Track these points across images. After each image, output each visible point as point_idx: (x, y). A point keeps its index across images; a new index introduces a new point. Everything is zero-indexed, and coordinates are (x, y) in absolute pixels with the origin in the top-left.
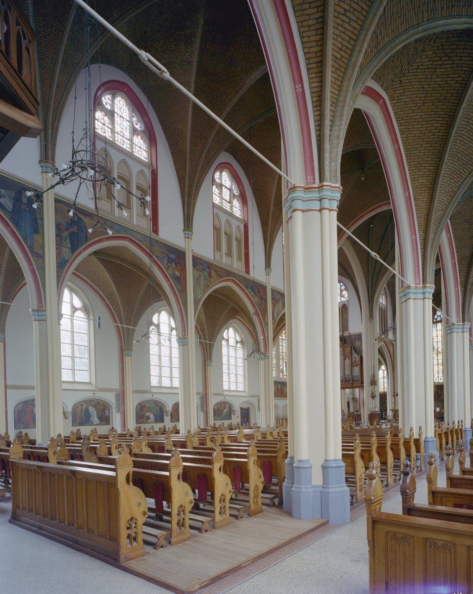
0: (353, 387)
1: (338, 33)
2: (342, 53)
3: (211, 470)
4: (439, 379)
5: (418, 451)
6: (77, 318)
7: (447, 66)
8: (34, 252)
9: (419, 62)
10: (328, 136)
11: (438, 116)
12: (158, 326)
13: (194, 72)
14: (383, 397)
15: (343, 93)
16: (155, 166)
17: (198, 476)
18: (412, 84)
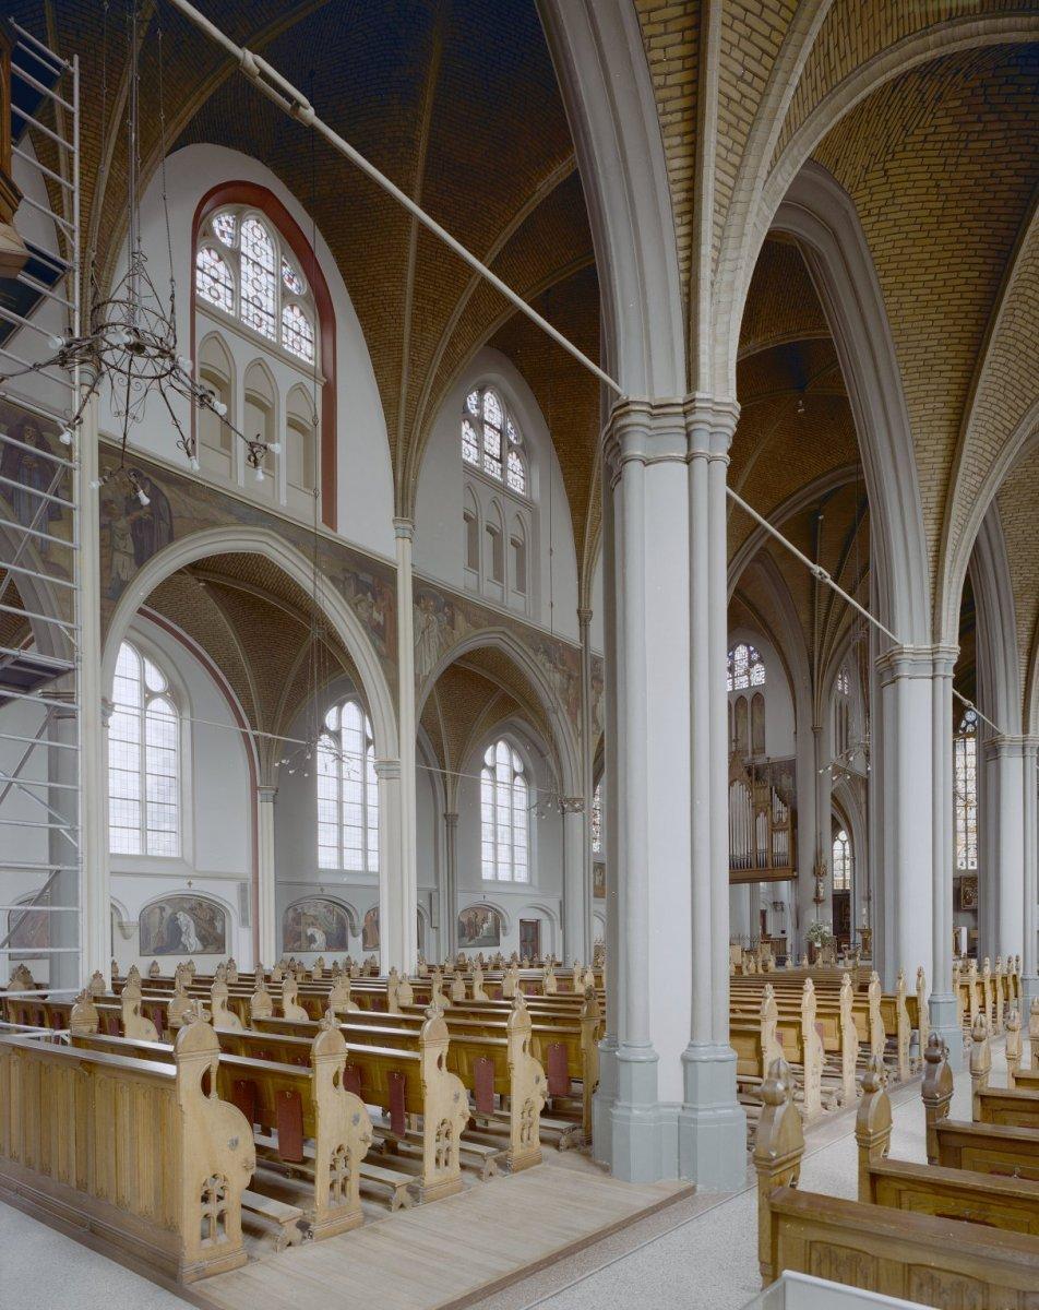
0: (754, 880)
1: (734, 38)
2: (742, 87)
3: (417, 1063)
4: (969, 862)
5: (915, 1026)
6: (154, 715)
7: (995, 136)
8: (48, 562)
9: (929, 126)
10: (709, 285)
11: (972, 253)
12: (337, 736)
13: (421, 164)
14: (841, 902)
15: (744, 184)
16: (331, 375)
17: (390, 1074)
18: (912, 177)
